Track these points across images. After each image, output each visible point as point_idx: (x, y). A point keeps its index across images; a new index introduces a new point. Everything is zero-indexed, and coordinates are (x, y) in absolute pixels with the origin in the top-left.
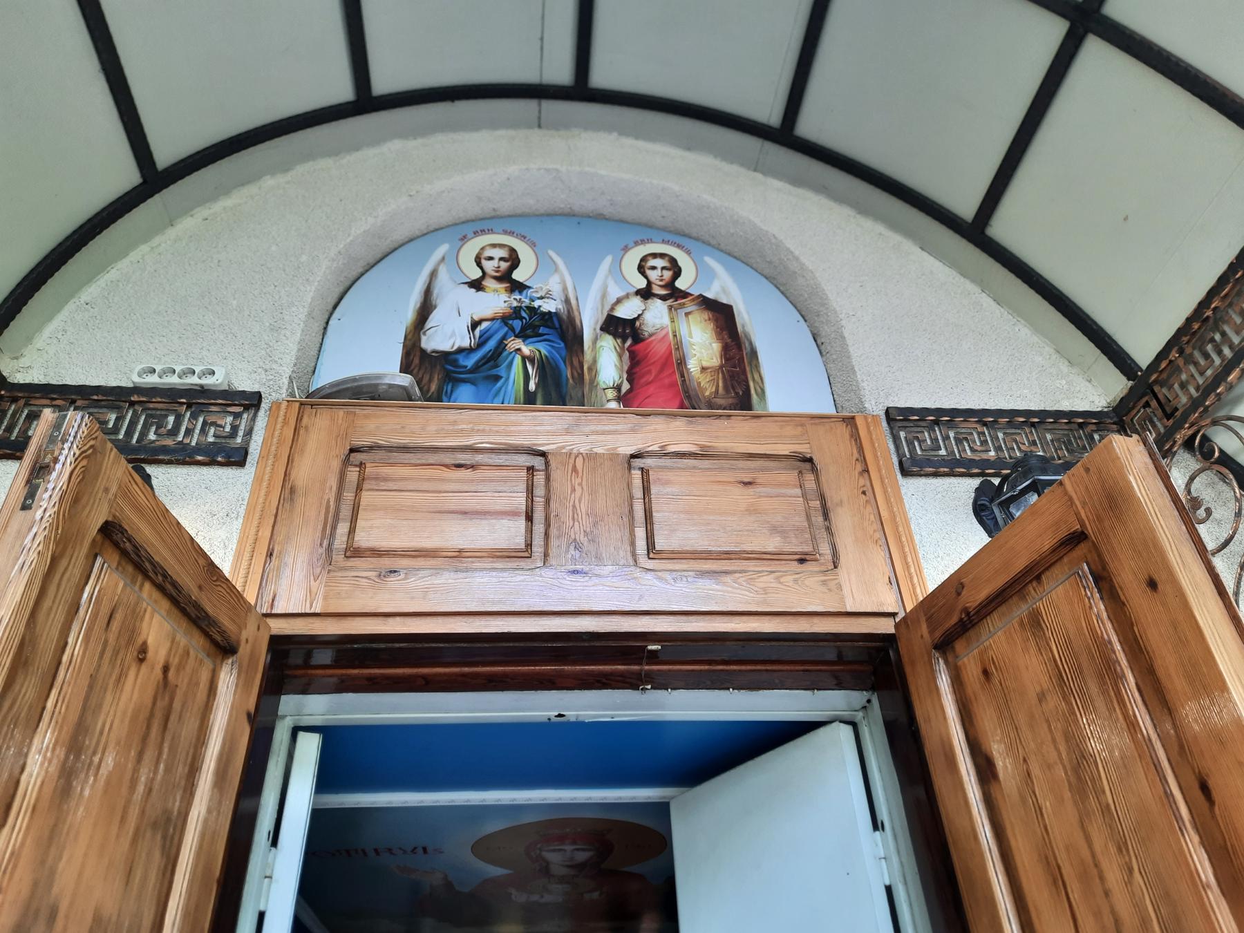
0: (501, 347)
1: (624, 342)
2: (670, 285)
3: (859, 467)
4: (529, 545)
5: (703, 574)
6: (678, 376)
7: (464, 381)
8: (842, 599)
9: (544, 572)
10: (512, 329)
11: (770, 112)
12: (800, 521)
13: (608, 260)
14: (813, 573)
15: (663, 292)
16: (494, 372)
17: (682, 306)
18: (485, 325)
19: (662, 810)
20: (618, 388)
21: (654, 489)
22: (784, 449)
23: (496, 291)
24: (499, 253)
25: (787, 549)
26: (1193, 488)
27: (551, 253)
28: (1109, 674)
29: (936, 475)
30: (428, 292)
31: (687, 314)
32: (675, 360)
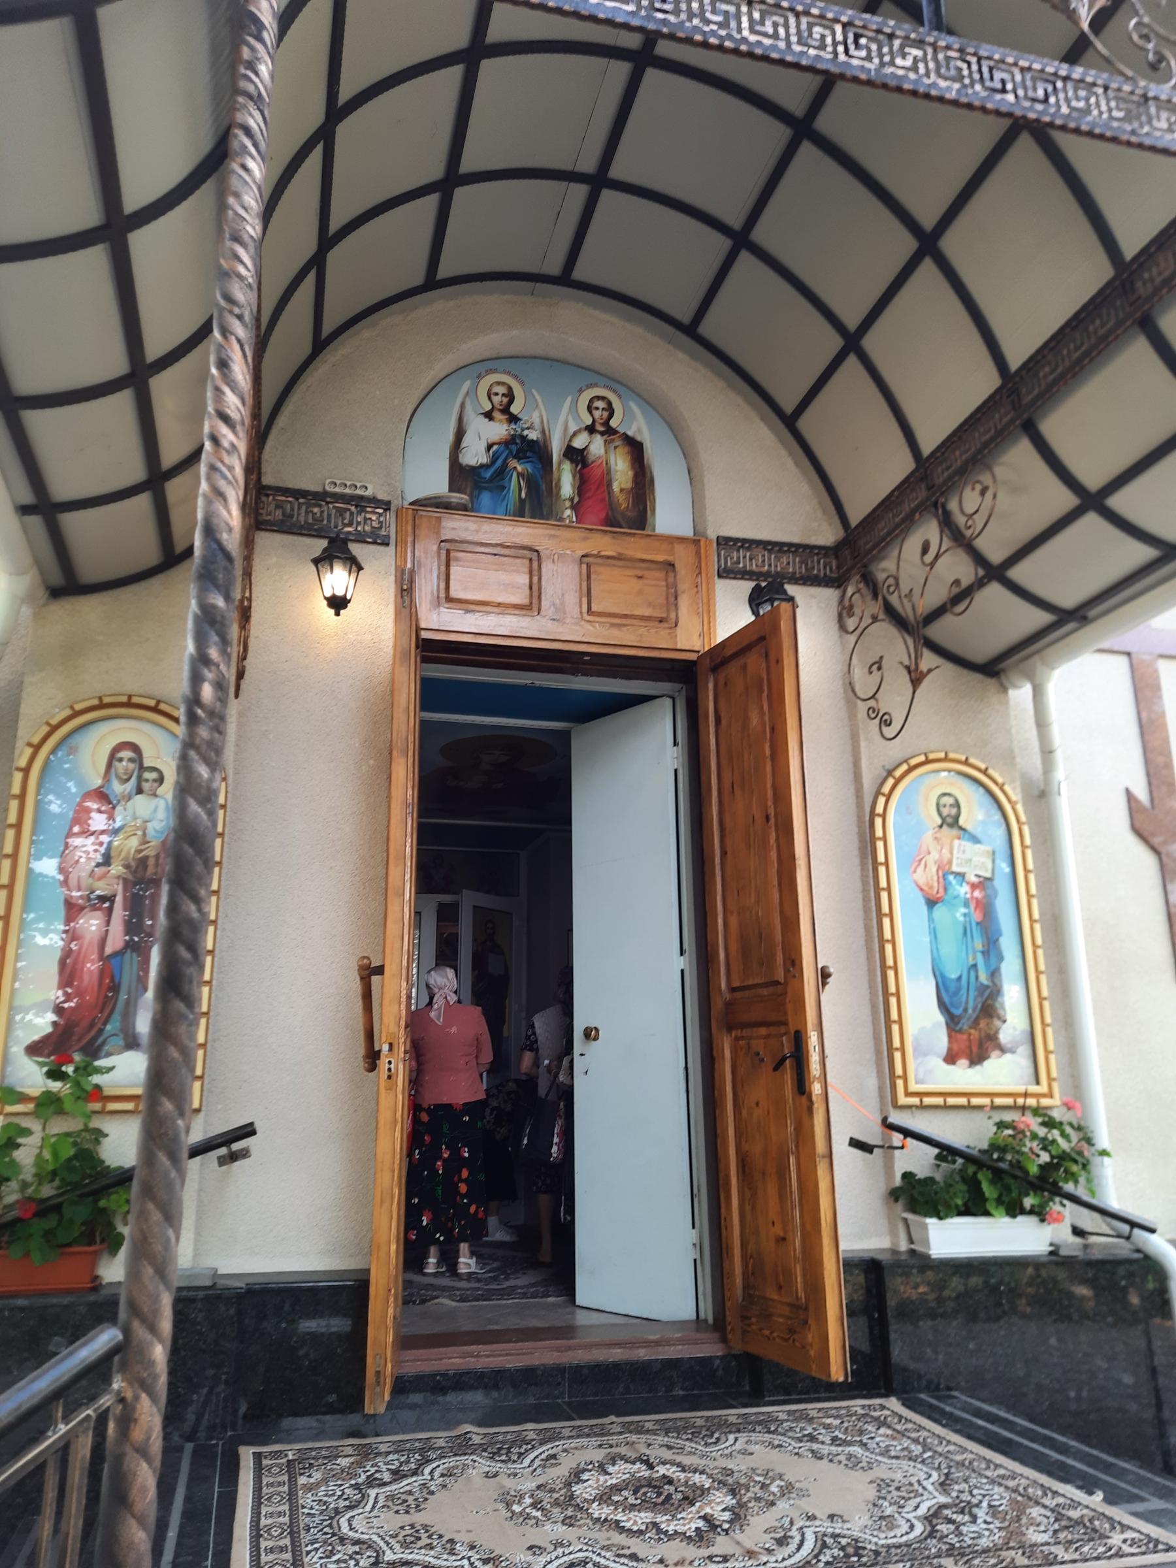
0: (505, 465)
1: (577, 466)
2: (606, 423)
3: (697, 572)
4: (531, 603)
5: (613, 625)
6: (606, 493)
7: (486, 489)
8: (676, 643)
9: (538, 617)
10: (511, 452)
11: (686, 319)
12: (662, 600)
13: (569, 399)
14: (665, 628)
15: (601, 429)
16: (501, 483)
17: (613, 441)
18: (495, 447)
19: (564, 738)
20: (572, 500)
21: (593, 577)
22: (660, 558)
23: (500, 421)
24: (501, 390)
25: (655, 615)
26: (853, 598)
27: (534, 391)
28: (761, 690)
29: (735, 578)
30: (460, 420)
31: (615, 448)
32: (606, 481)
